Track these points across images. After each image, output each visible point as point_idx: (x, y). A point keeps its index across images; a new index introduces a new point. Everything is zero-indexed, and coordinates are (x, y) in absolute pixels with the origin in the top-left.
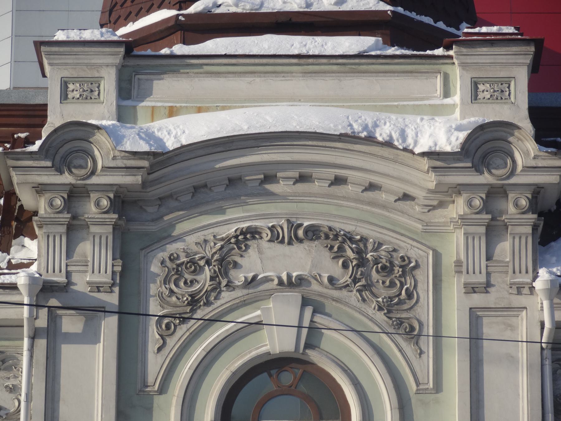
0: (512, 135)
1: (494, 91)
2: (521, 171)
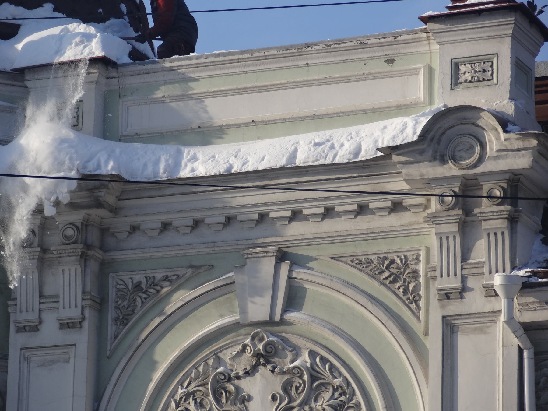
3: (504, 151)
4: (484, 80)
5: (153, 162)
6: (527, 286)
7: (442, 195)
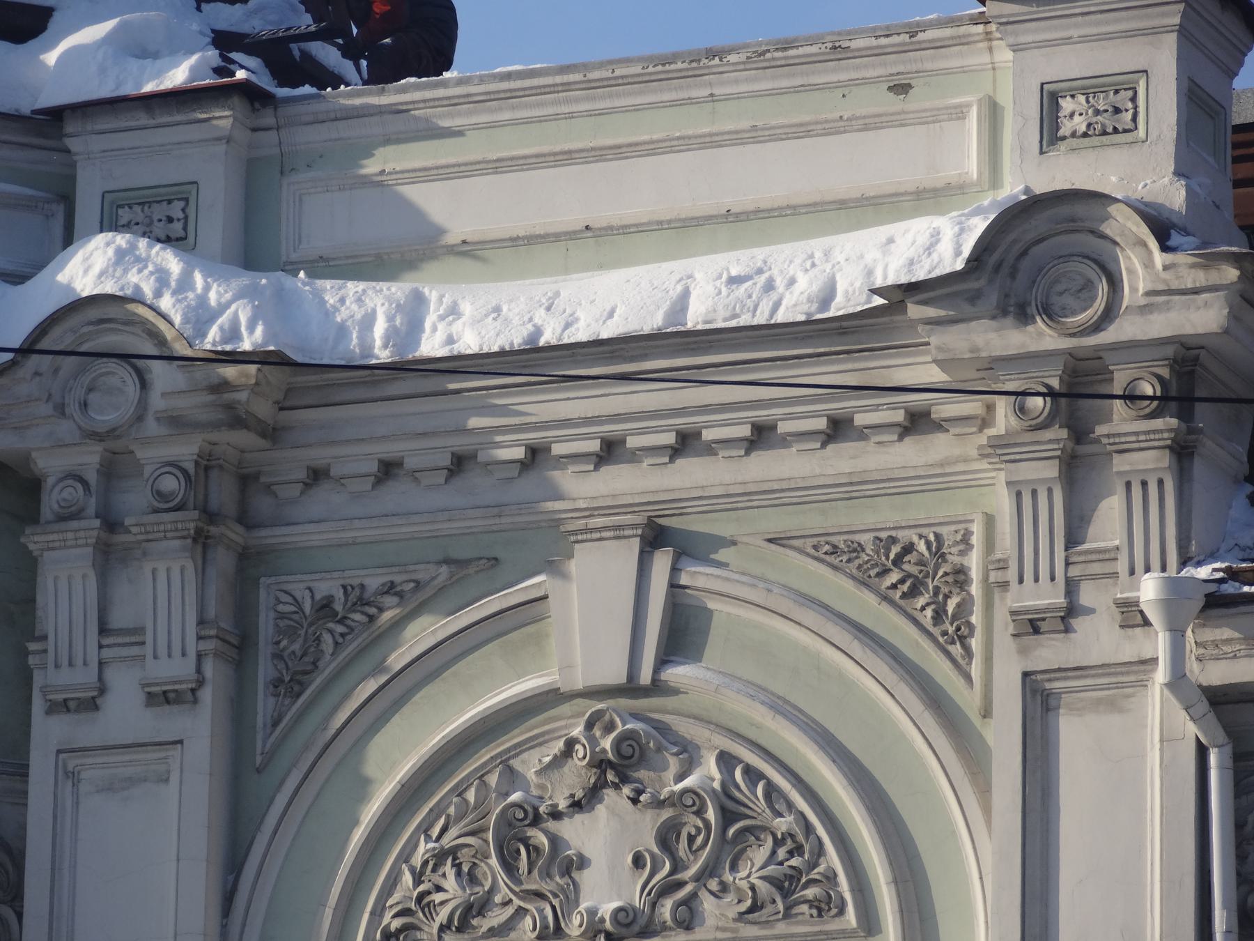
0: (1108, 217)
3: (1162, 294)
4: (1116, 130)
5: (364, 316)
6: (1216, 603)
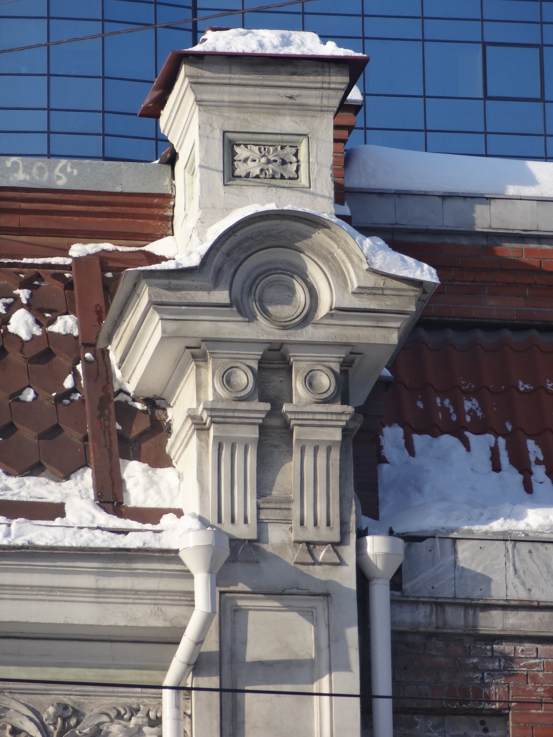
1: (269, 162)
2: (329, 315)
4: (282, 177)
7: (313, 564)
